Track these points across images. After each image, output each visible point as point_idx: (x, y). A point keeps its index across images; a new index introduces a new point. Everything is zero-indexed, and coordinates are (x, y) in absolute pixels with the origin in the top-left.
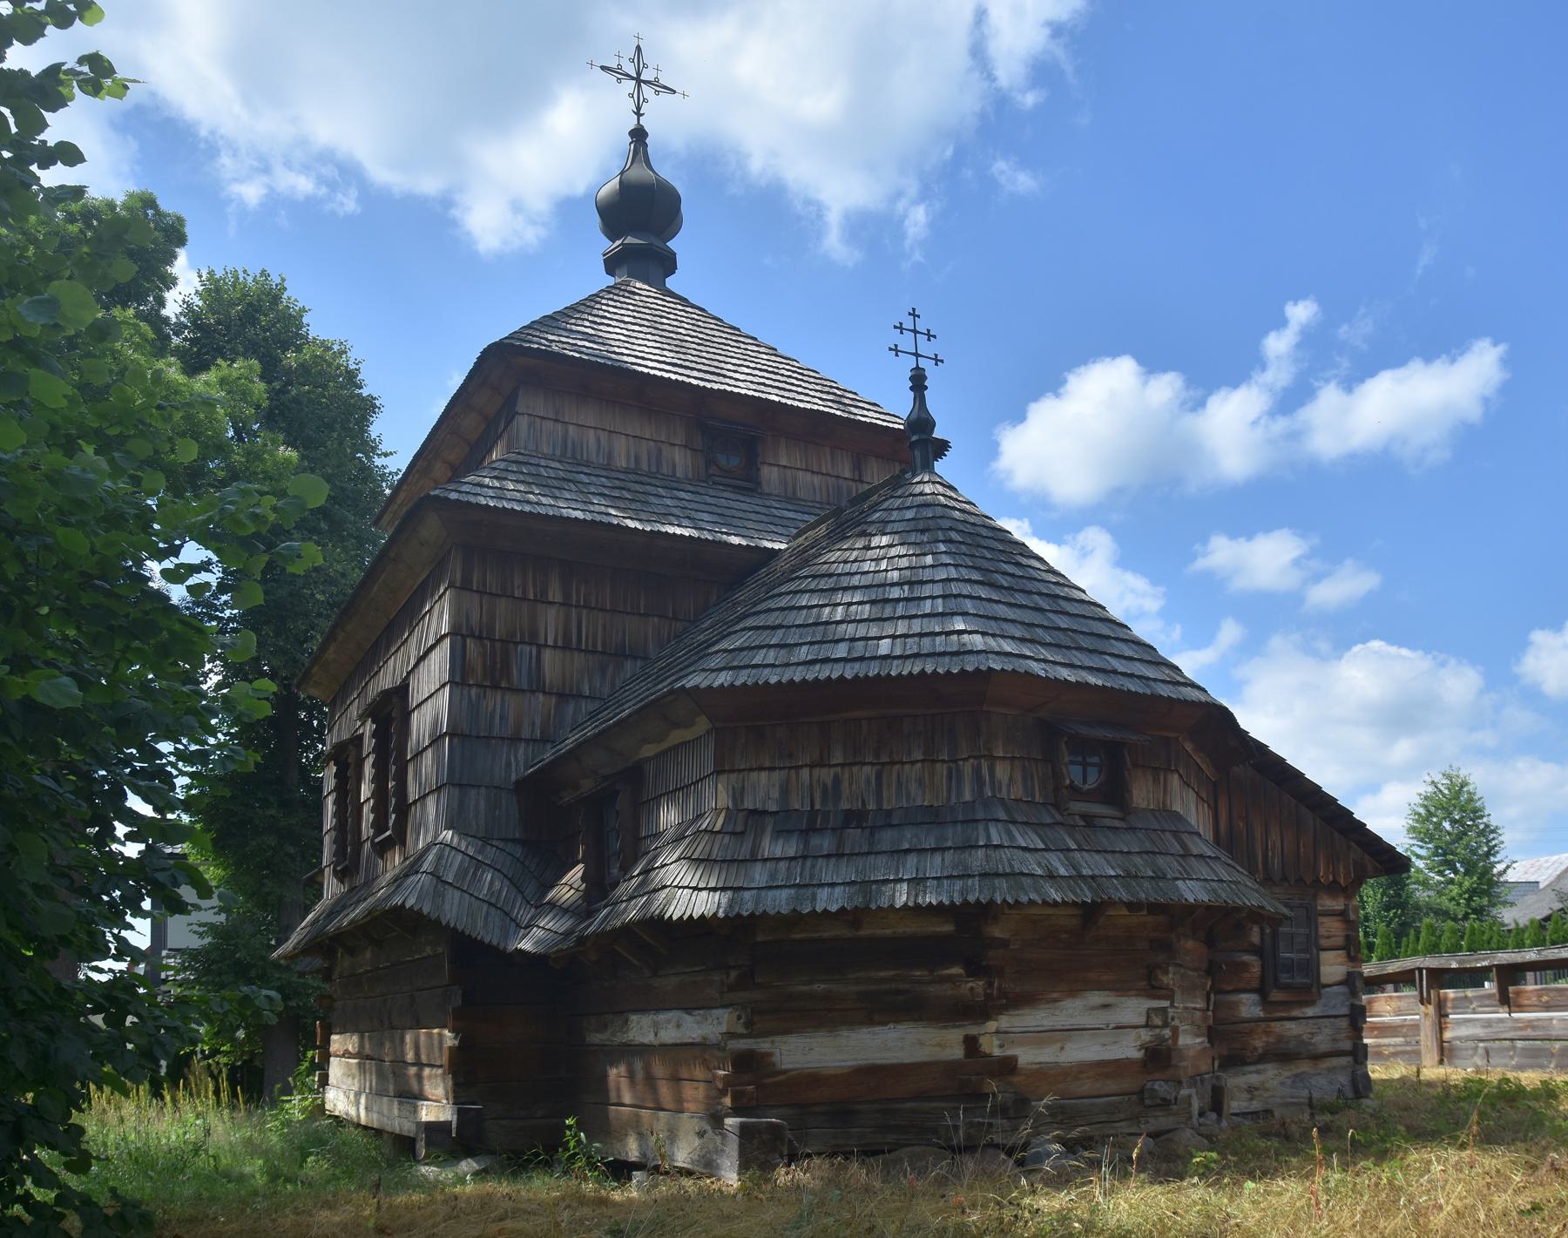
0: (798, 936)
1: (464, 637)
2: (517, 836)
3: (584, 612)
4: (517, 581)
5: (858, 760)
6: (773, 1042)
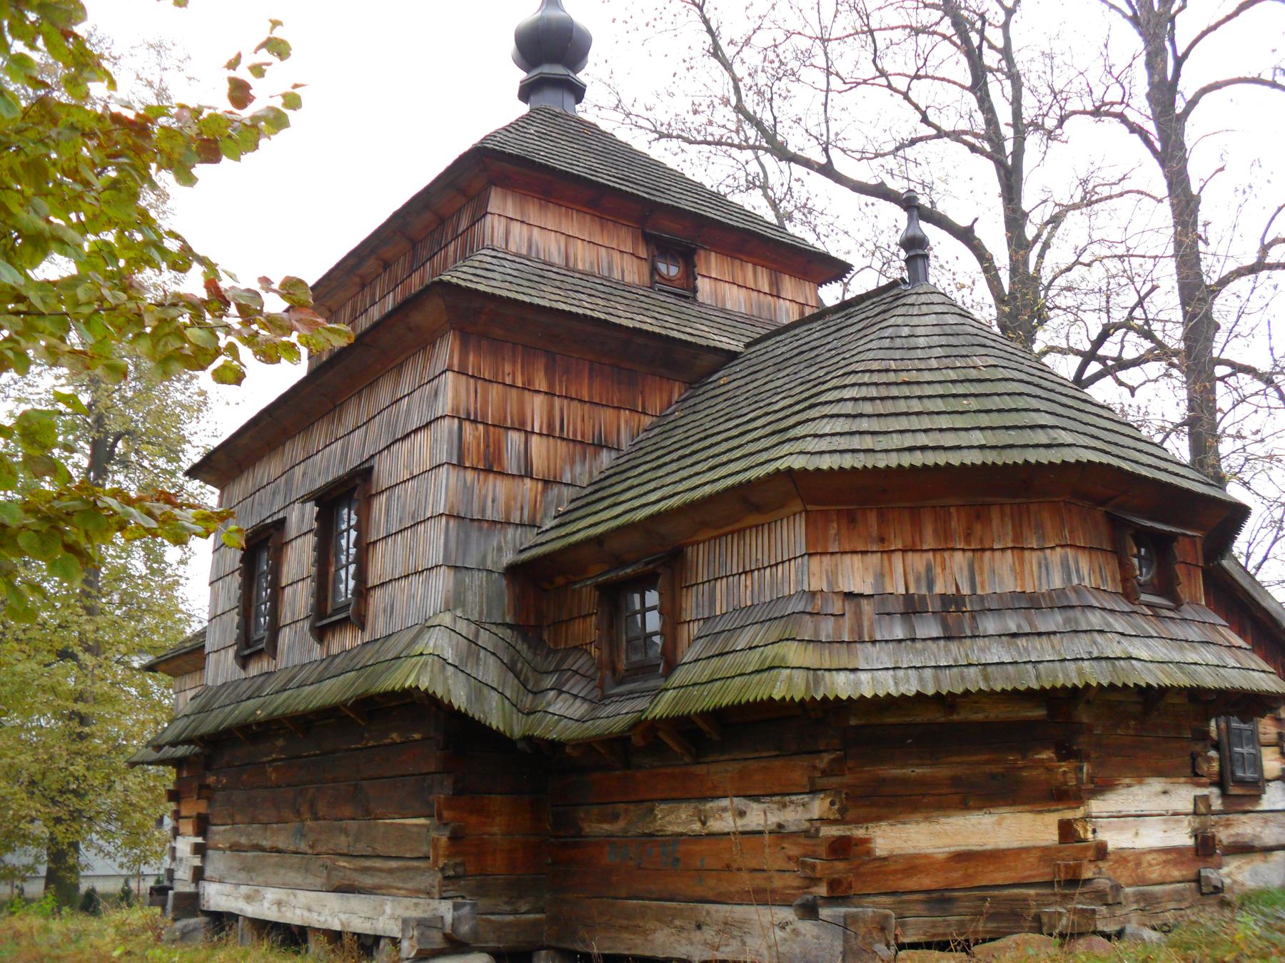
2: (508, 620)
3: (566, 402)
4: (508, 368)
6: (867, 828)
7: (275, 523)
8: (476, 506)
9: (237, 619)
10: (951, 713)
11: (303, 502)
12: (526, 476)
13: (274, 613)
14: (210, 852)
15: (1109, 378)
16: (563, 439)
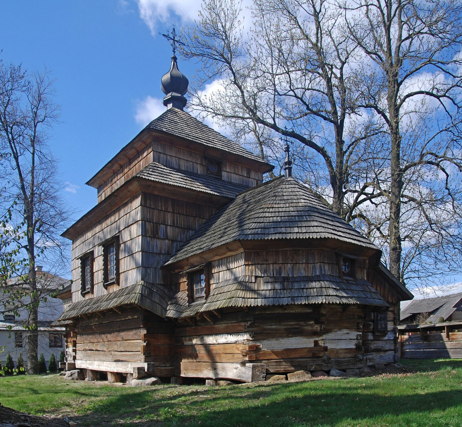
0: (268, 312)
1: (145, 221)
2: (161, 283)
3: (178, 215)
4: (160, 204)
5: (287, 262)
7: (90, 252)
8: (151, 249)
9: (81, 282)
10: (285, 310)
11: (99, 246)
12: (166, 239)
13: (92, 280)
14: (77, 351)
15: (369, 201)
16: (177, 227)
